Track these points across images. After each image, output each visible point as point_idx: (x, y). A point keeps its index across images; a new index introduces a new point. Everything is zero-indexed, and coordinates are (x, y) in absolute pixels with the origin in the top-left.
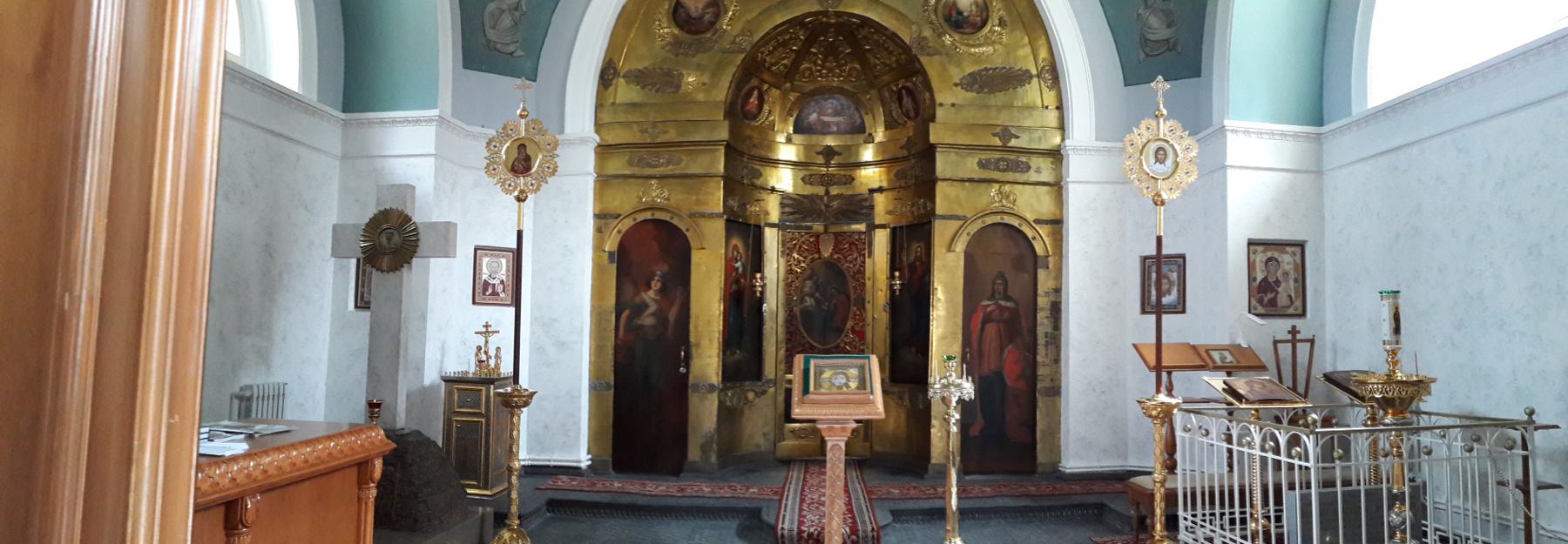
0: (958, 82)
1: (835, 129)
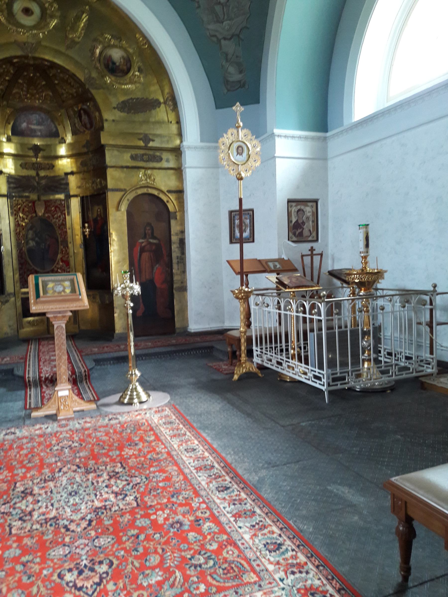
0: (116, 106)
1: (39, 134)
